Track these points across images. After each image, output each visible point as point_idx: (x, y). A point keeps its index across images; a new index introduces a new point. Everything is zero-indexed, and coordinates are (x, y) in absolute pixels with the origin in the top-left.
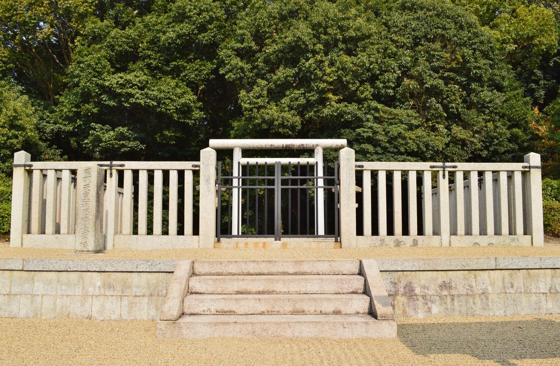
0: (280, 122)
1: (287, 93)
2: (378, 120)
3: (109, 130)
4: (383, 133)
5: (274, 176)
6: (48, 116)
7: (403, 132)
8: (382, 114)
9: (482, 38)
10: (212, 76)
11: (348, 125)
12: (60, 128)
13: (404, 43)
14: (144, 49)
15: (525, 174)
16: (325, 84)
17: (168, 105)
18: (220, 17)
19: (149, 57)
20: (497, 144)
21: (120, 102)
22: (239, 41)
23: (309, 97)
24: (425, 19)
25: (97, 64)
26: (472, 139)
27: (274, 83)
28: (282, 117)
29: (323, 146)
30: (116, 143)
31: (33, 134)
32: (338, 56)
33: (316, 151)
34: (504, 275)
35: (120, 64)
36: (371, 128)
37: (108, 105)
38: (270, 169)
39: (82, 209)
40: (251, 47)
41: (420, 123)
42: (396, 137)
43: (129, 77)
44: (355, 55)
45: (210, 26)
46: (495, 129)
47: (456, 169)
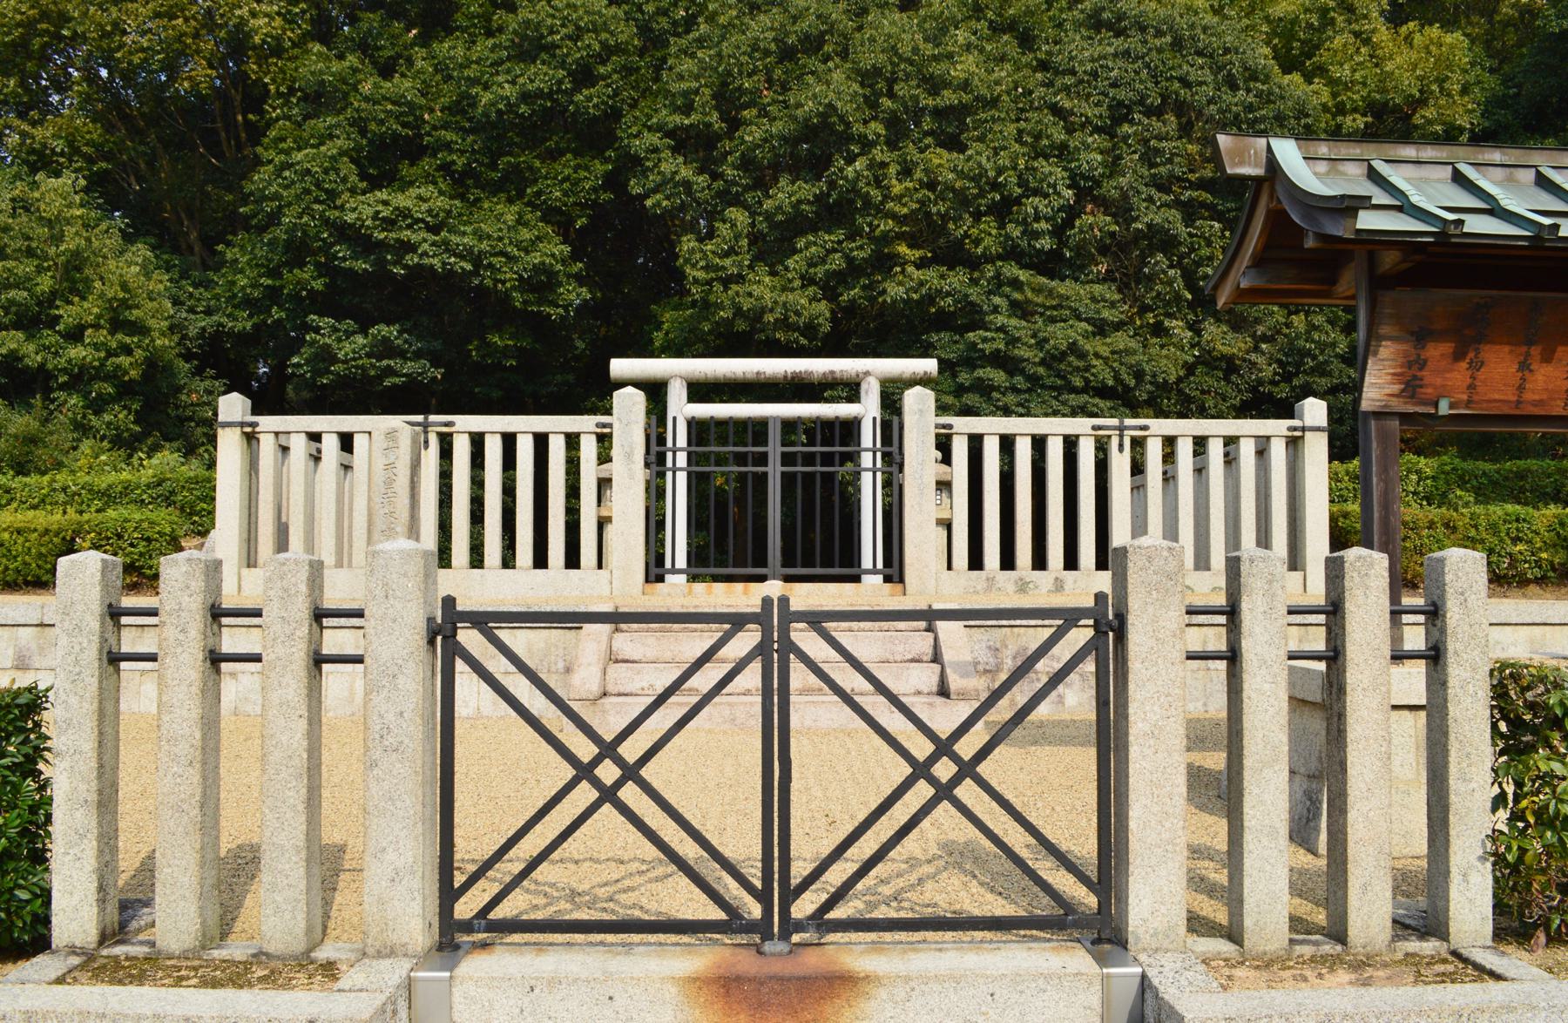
0: (779, 316)
1: (801, 244)
2: (1021, 310)
3: (354, 333)
4: (1033, 341)
5: (766, 445)
6: (191, 295)
7: (1081, 341)
8: (1029, 294)
9: (1281, 105)
10: (605, 196)
11: (944, 321)
12: (220, 324)
13: (1087, 117)
14: (435, 128)
15: (1294, 443)
16: (890, 222)
17: (499, 270)
18: (627, 43)
19: (448, 146)
20: (1313, 371)
21: (381, 264)
22: (676, 109)
23: (852, 250)
24: (1143, 58)
25: (326, 171)
26: (1253, 357)
27: (766, 219)
28: (785, 304)
29: (881, 376)
30: (371, 364)
31: (167, 342)
32: (922, 151)
33: (864, 386)
34: (1206, 636)
35: (378, 167)
36: (1002, 329)
37: (351, 269)
38: (759, 428)
39: (382, 512)
40: (709, 125)
41: (1123, 316)
42: (1064, 354)
43: (403, 200)
44: (962, 148)
45: (602, 70)
46: (1308, 332)
47: (1146, 433)
